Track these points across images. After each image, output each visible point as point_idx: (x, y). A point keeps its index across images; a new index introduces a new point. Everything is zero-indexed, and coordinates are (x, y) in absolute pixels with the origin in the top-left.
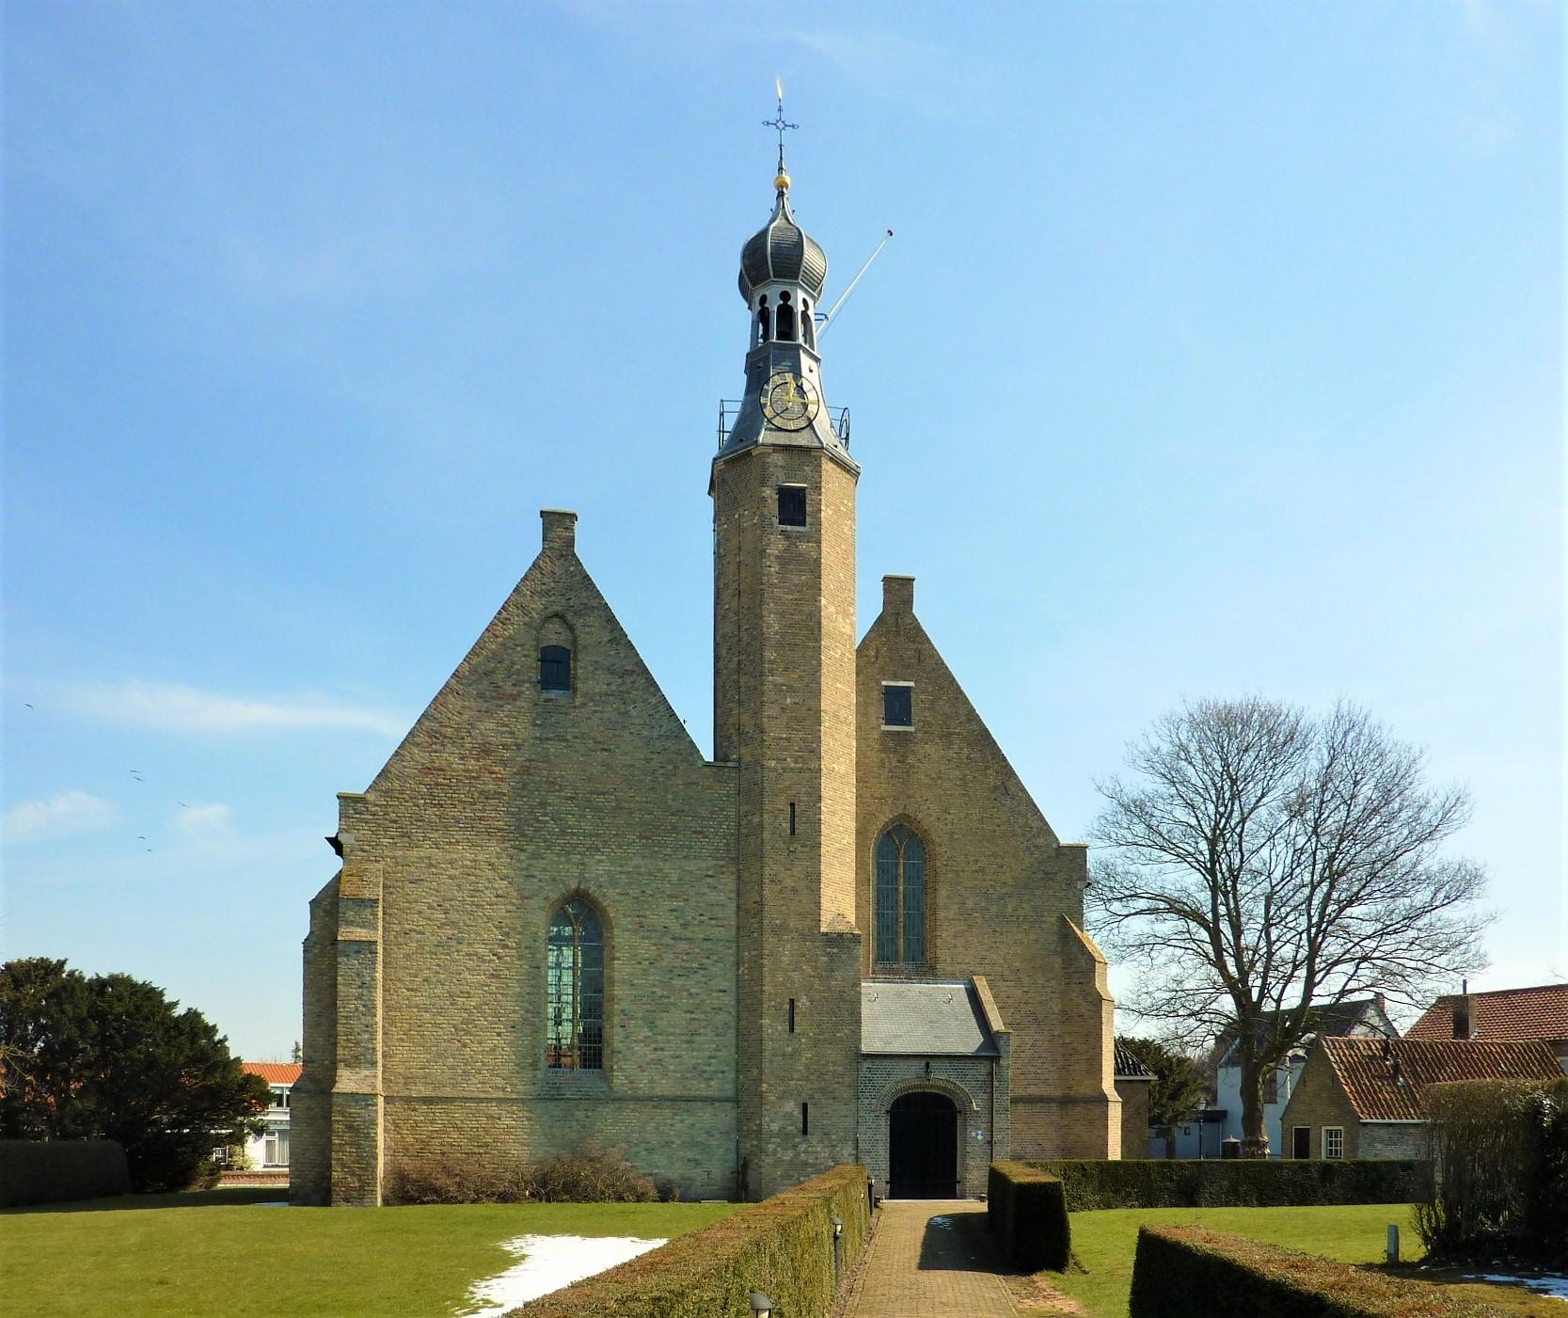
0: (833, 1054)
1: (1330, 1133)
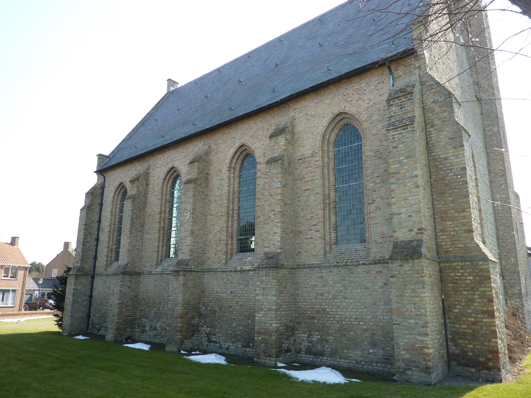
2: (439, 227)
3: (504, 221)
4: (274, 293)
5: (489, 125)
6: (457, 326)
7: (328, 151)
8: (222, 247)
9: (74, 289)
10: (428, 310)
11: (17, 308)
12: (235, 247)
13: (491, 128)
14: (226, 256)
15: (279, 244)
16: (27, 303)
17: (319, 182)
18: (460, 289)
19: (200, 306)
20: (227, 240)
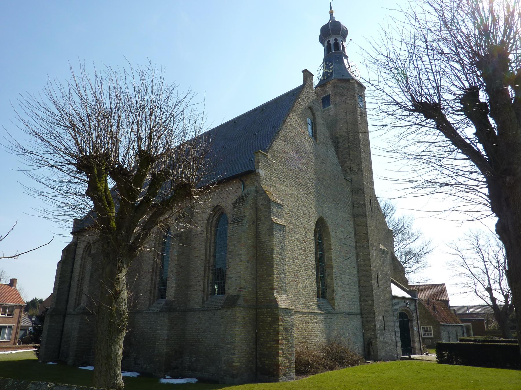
0: (388, 297)
1: (424, 328)
2: (258, 286)
4: (166, 328)
6: (262, 349)
7: (211, 230)
9: (49, 326)
11: (12, 342)
12: (156, 295)
15: (173, 295)
16: (21, 338)
17: (203, 251)
20: (151, 290)
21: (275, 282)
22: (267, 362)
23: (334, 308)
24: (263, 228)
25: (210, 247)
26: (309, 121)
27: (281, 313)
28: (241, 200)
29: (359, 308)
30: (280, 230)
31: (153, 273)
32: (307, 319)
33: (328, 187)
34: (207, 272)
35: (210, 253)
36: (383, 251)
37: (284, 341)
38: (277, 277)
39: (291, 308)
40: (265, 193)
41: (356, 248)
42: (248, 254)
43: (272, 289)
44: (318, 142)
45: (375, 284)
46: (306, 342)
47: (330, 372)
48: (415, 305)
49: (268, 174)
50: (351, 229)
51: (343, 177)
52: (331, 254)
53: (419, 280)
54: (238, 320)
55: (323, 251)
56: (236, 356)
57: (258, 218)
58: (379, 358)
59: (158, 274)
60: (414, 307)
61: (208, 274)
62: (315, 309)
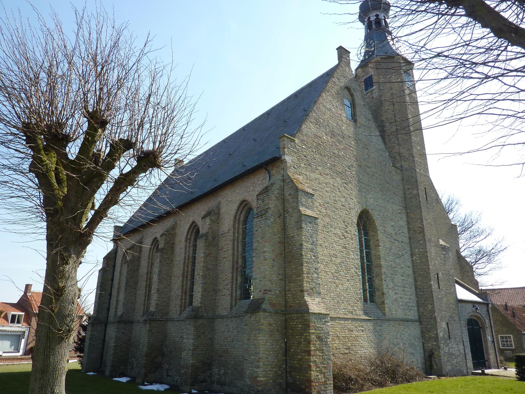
0: (452, 301)
1: (502, 337)
2: (287, 288)
3: (422, 273)
5: (409, 189)
7: (238, 228)
8: (178, 302)
9: (90, 335)
10: (261, 349)
12: (187, 301)
13: (411, 191)
14: (181, 308)
15: (200, 300)
17: (230, 252)
18: (295, 334)
19: (164, 347)
20: (182, 296)
21: (305, 282)
22: (298, 377)
23: (384, 314)
24: (291, 221)
25: (238, 246)
26: (347, 103)
27: (313, 319)
28: (266, 190)
29: (416, 314)
30: (310, 223)
31: (183, 277)
32: (350, 326)
33: (373, 175)
34: (235, 275)
35: (238, 253)
36: (444, 248)
37: (318, 352)
38: (308, 277)
39: (325, 313)
40: (292, 181)
41: (410, 245)
42: (273, 251)
43: (302, 291)
44: (358, 125)
45: (435, 286)
46: (350, 353)
47: (378, 390)
48: (488, 311)
49: (296, 161)
50: (403, 223)
51: (391, 164)
52: (379, 251)
53: (493, 282)
54: (263, 327)
55: (370, 249)
56: (261, 370)
57: (285, 210)
58: (444, 373)
59: (189, 278)
60: (486, 312)
61: (237, 276)
62: (360, 315)
